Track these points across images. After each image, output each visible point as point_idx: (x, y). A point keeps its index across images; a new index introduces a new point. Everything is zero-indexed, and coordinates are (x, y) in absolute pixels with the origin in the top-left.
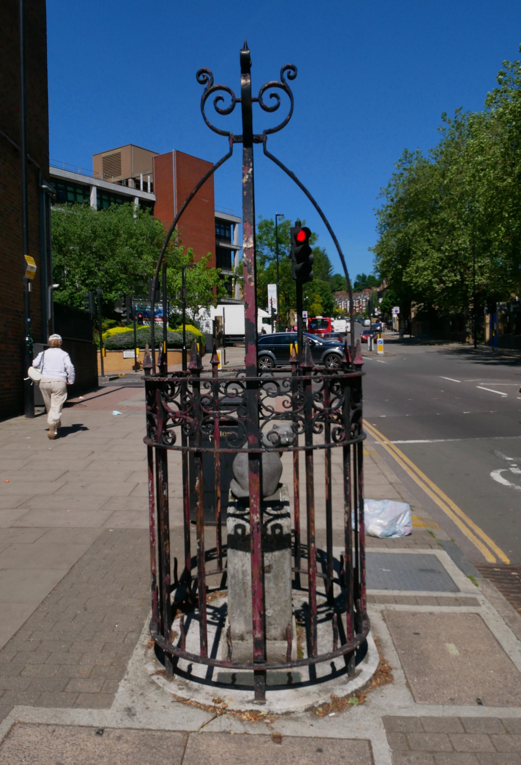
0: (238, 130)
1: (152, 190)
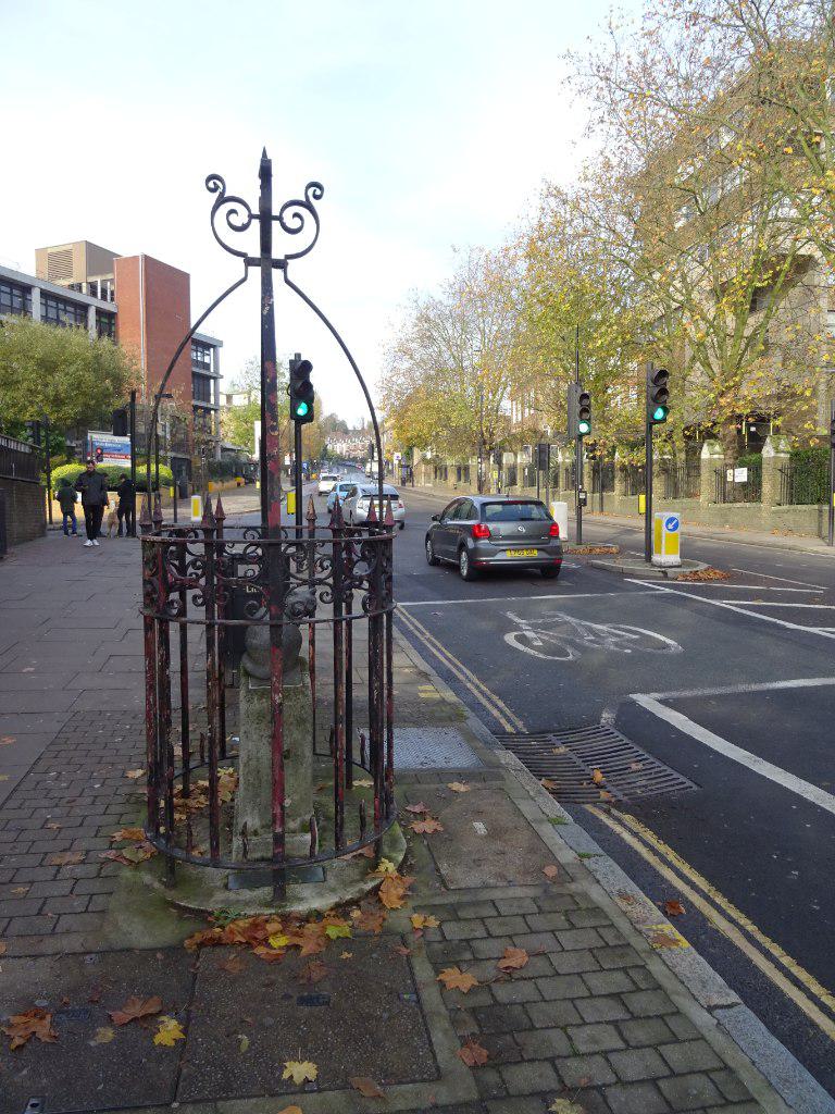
0: (255, 251)
1: (112, 300)
